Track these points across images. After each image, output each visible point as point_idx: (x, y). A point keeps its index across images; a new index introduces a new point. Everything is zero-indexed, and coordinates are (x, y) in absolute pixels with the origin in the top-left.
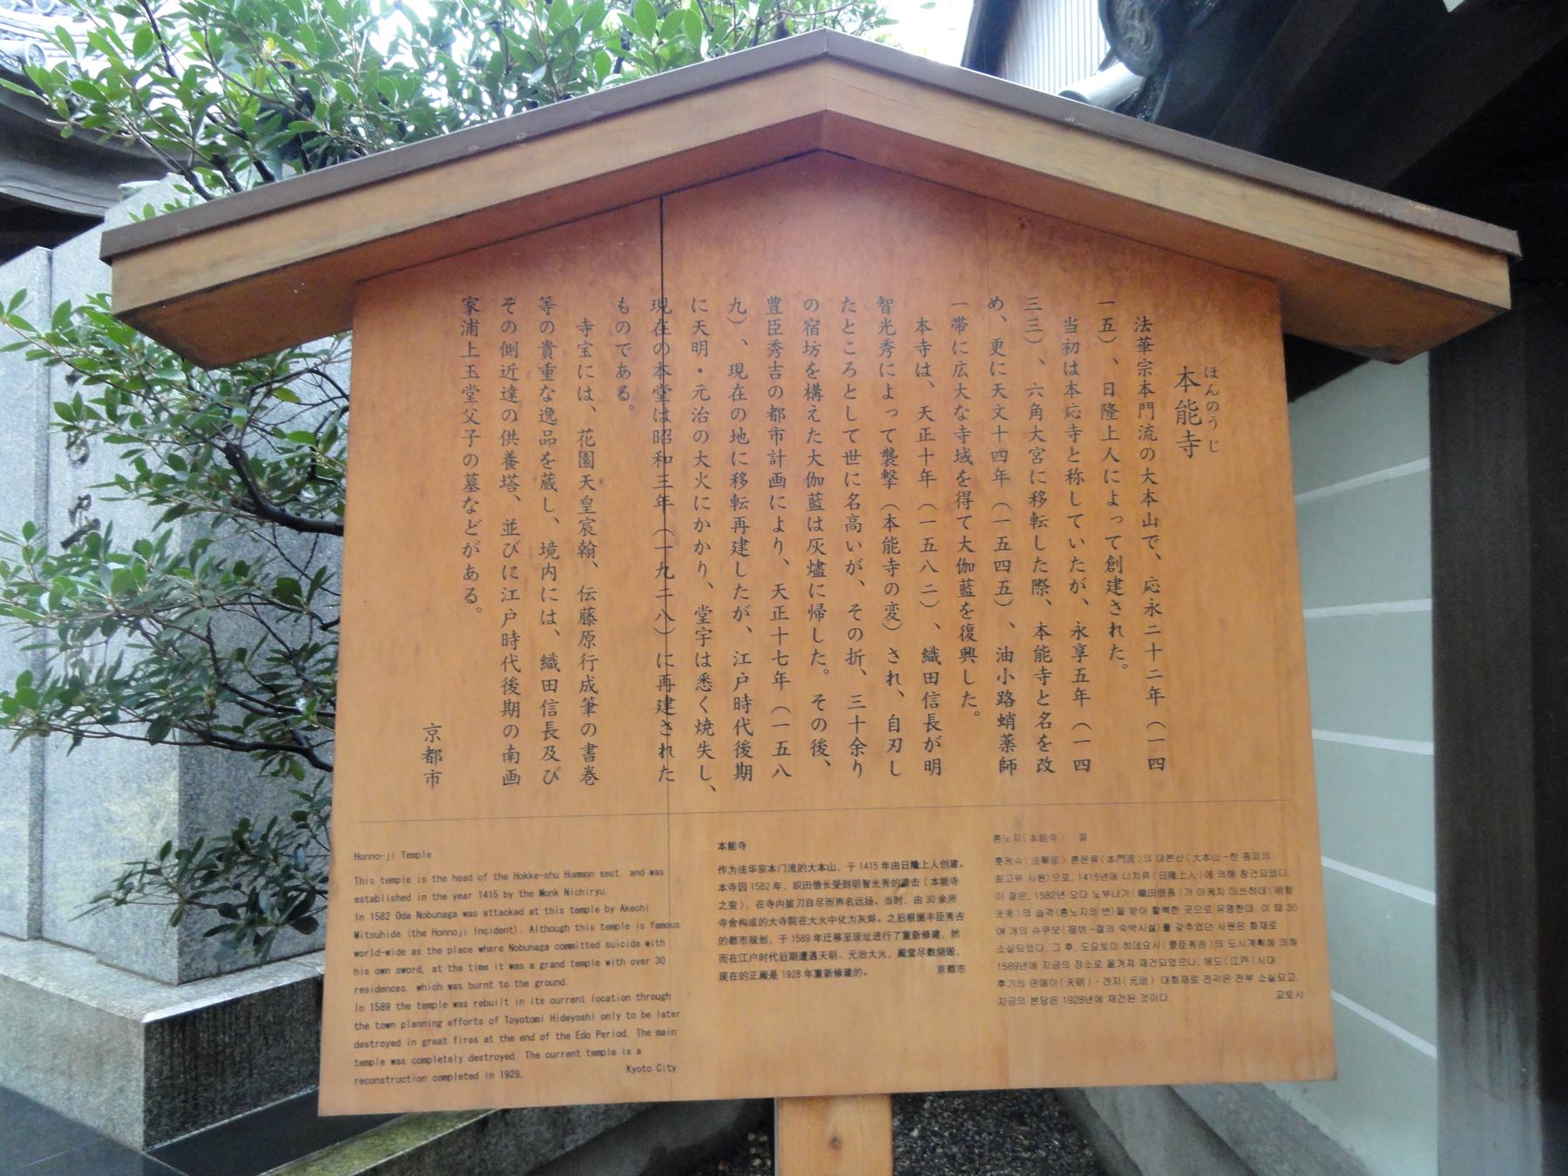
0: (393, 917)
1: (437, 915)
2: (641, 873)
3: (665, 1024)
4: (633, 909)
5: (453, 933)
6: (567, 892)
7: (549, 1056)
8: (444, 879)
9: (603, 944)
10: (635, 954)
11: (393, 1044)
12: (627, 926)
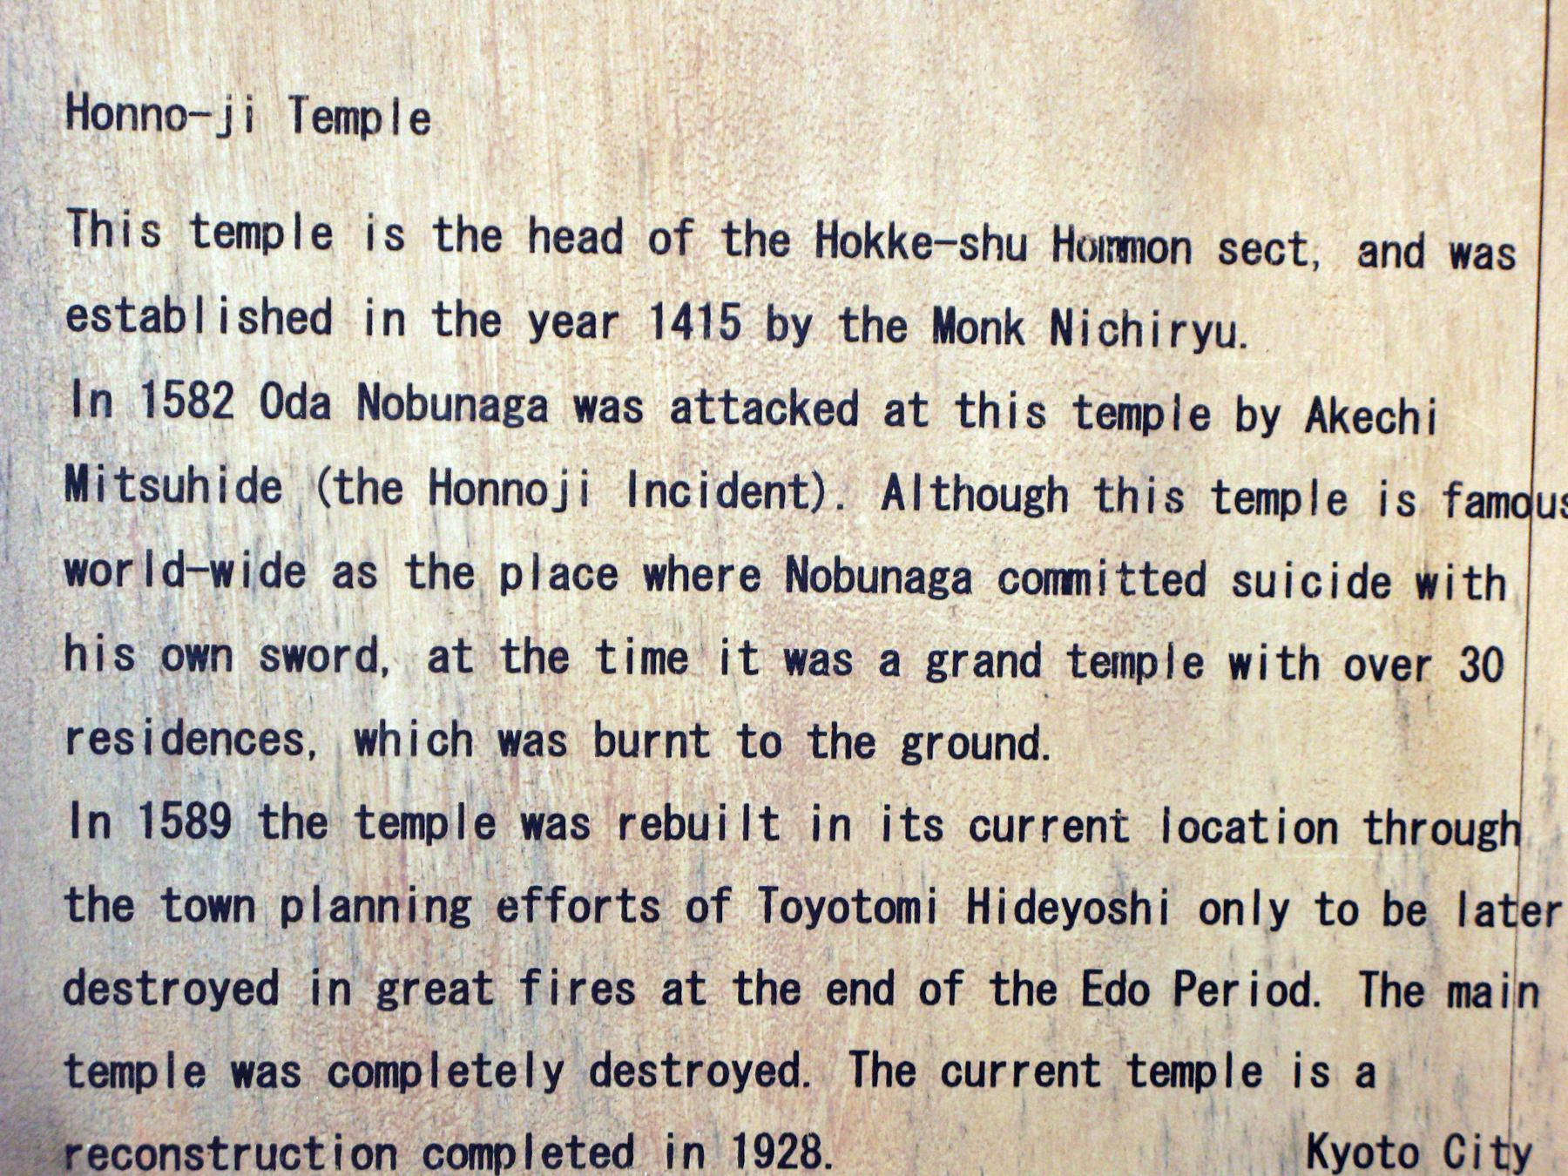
0: (245, 405)
1: (454, 407)
2: (1412, 255)
3: (1487, 955)
4: (1364, 420)
5: (529, 493)
6: (1061, 327)
7: (957, 1075)
8: (490, 239)
9: (1220, 580)
10: (1373, 628)
11: (244, 991)
12: (1337, 501)
